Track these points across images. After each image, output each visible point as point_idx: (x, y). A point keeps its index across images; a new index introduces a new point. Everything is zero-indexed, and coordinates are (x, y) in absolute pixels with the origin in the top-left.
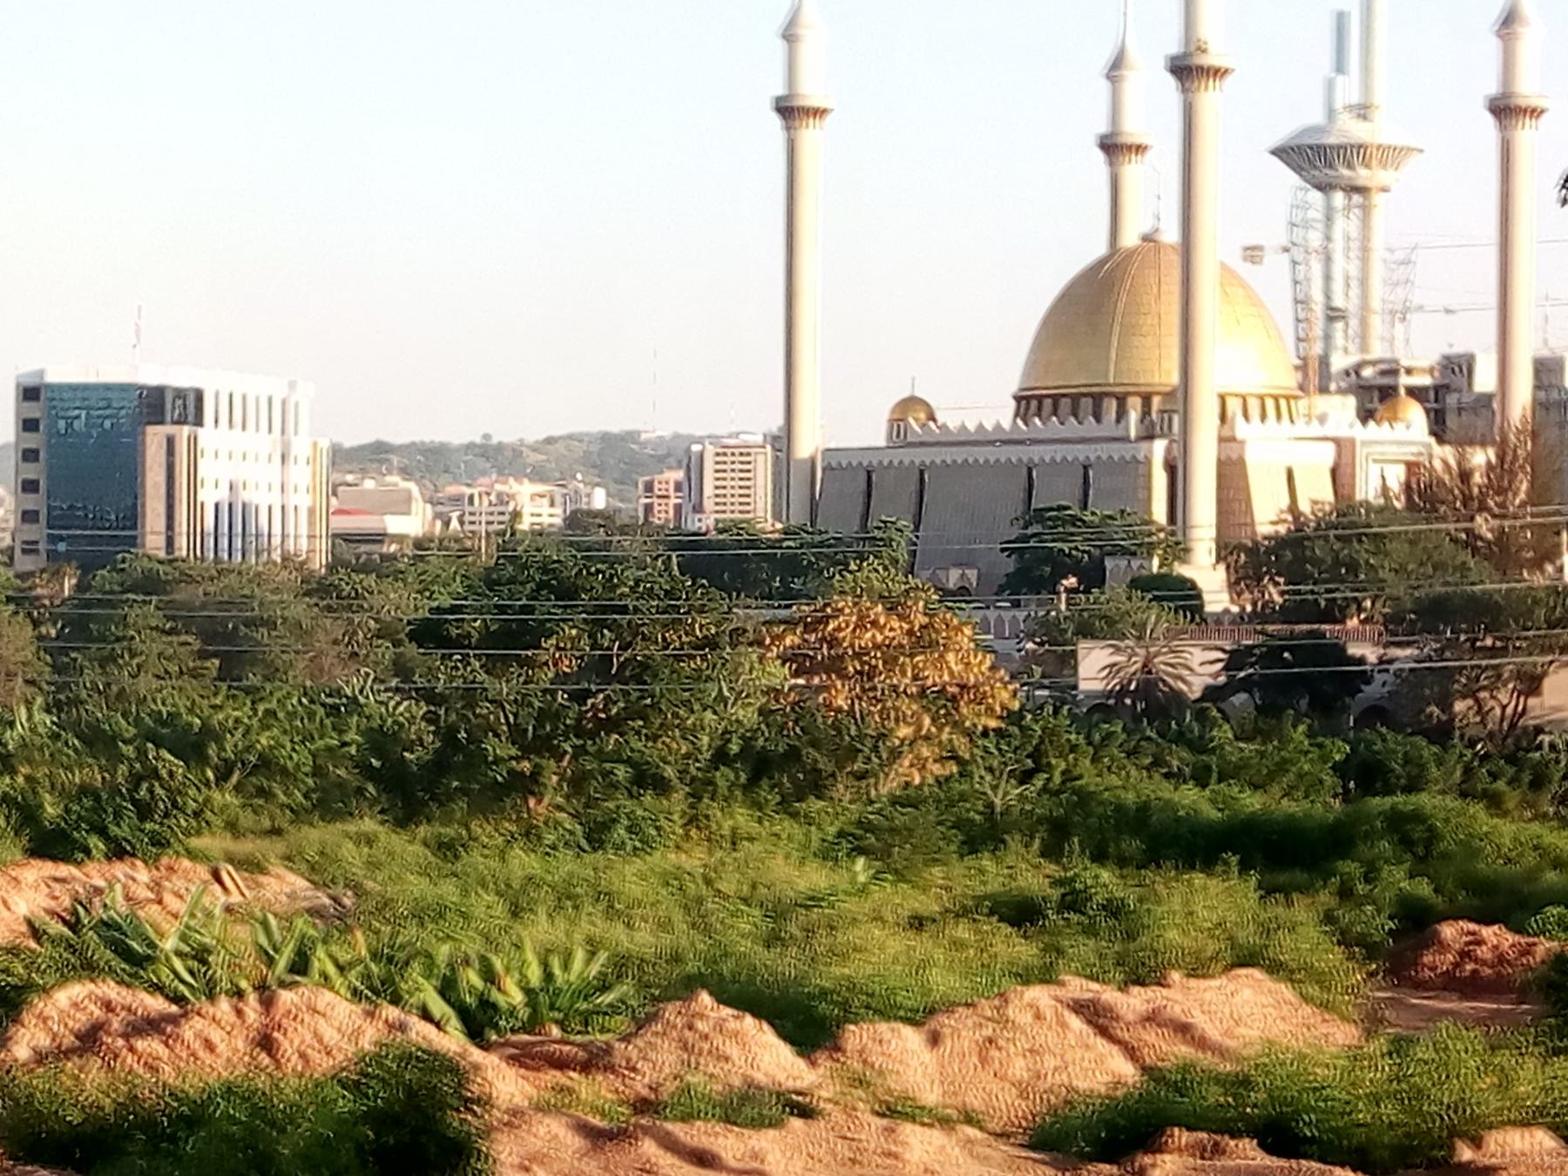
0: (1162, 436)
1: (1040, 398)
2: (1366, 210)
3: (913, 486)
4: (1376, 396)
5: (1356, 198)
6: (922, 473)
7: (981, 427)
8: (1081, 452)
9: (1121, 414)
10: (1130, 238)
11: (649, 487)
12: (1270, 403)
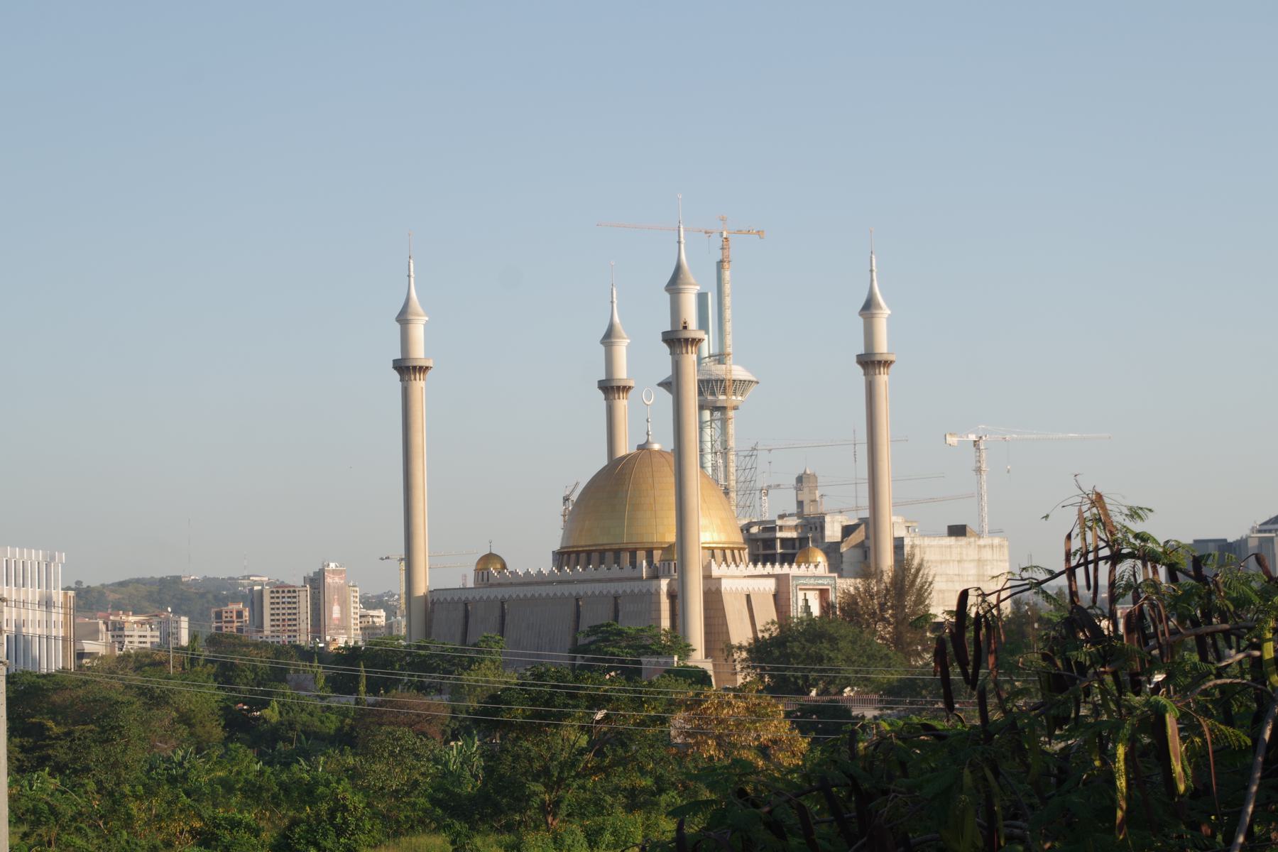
0: (665, 577)
1: (578, 553)
2: (724, 422)
3: (497, 613)
5: (717, 414)
6: (502, 603)
7: (528, 573)
8: (613, 588)
9: (633, 564)
10: (625, 447)
11: (219, 616)
12: (728, 553)
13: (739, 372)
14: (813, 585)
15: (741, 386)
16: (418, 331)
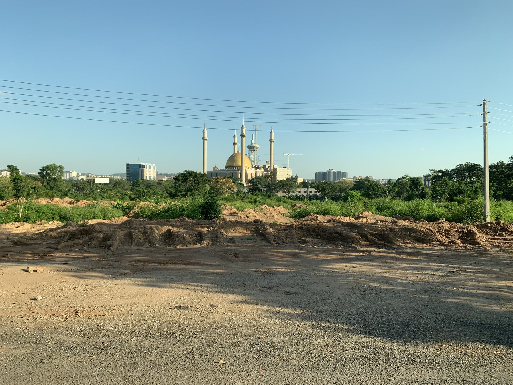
4: (258, 168)
13: (257, 146)
14: (261, 172)
15: (257, 147)
16: (273, 136)
